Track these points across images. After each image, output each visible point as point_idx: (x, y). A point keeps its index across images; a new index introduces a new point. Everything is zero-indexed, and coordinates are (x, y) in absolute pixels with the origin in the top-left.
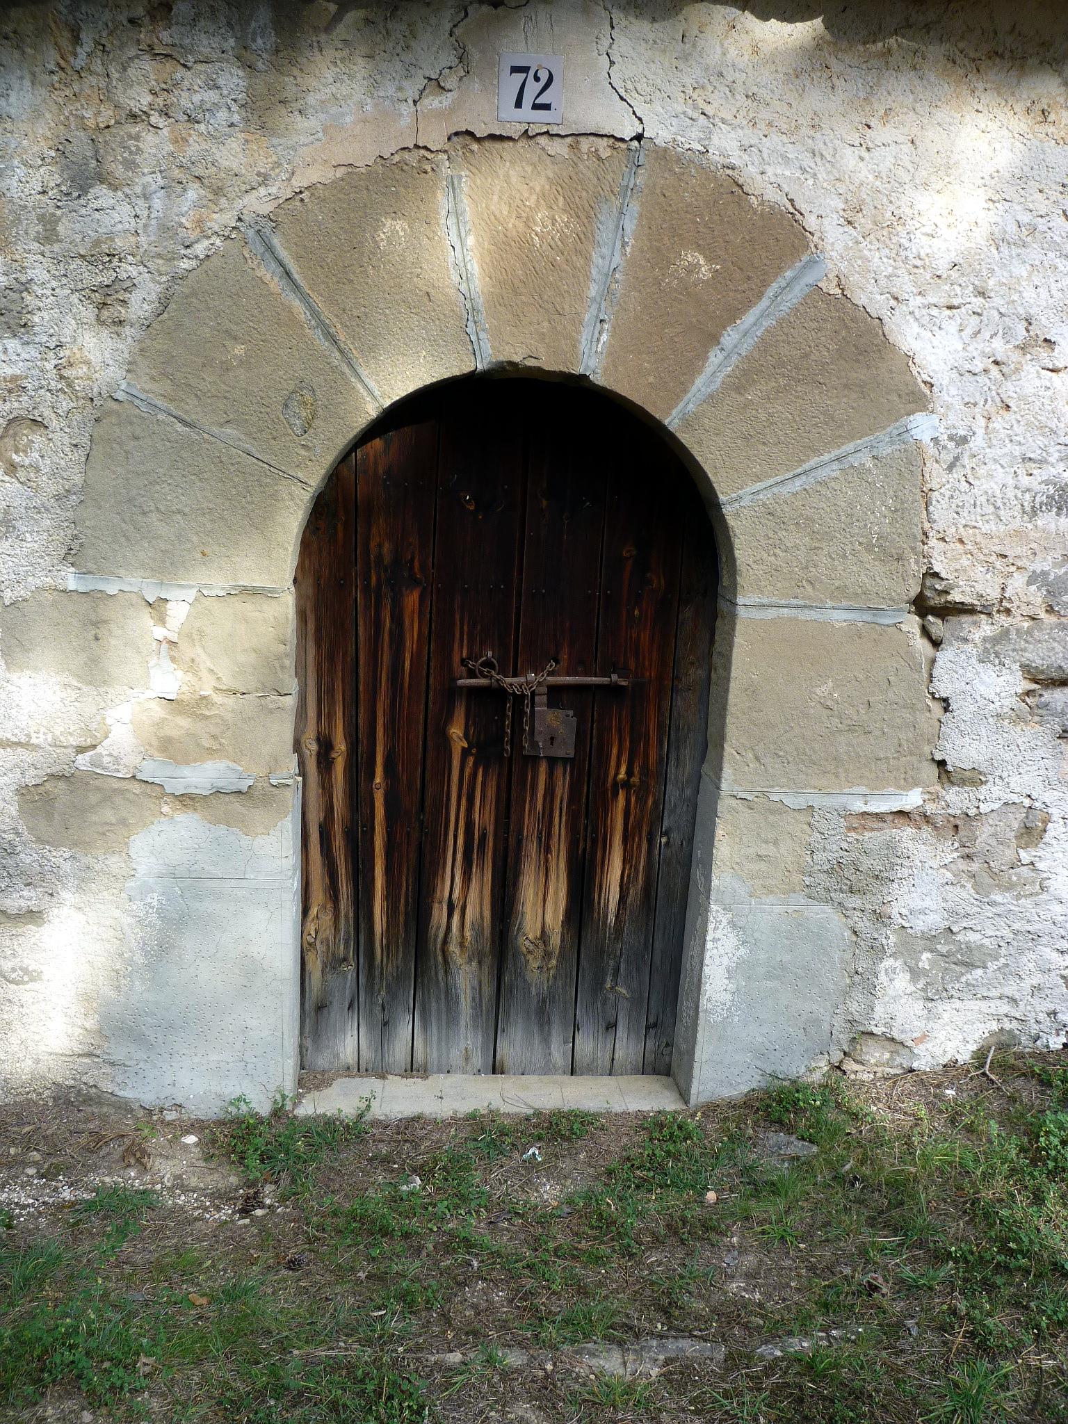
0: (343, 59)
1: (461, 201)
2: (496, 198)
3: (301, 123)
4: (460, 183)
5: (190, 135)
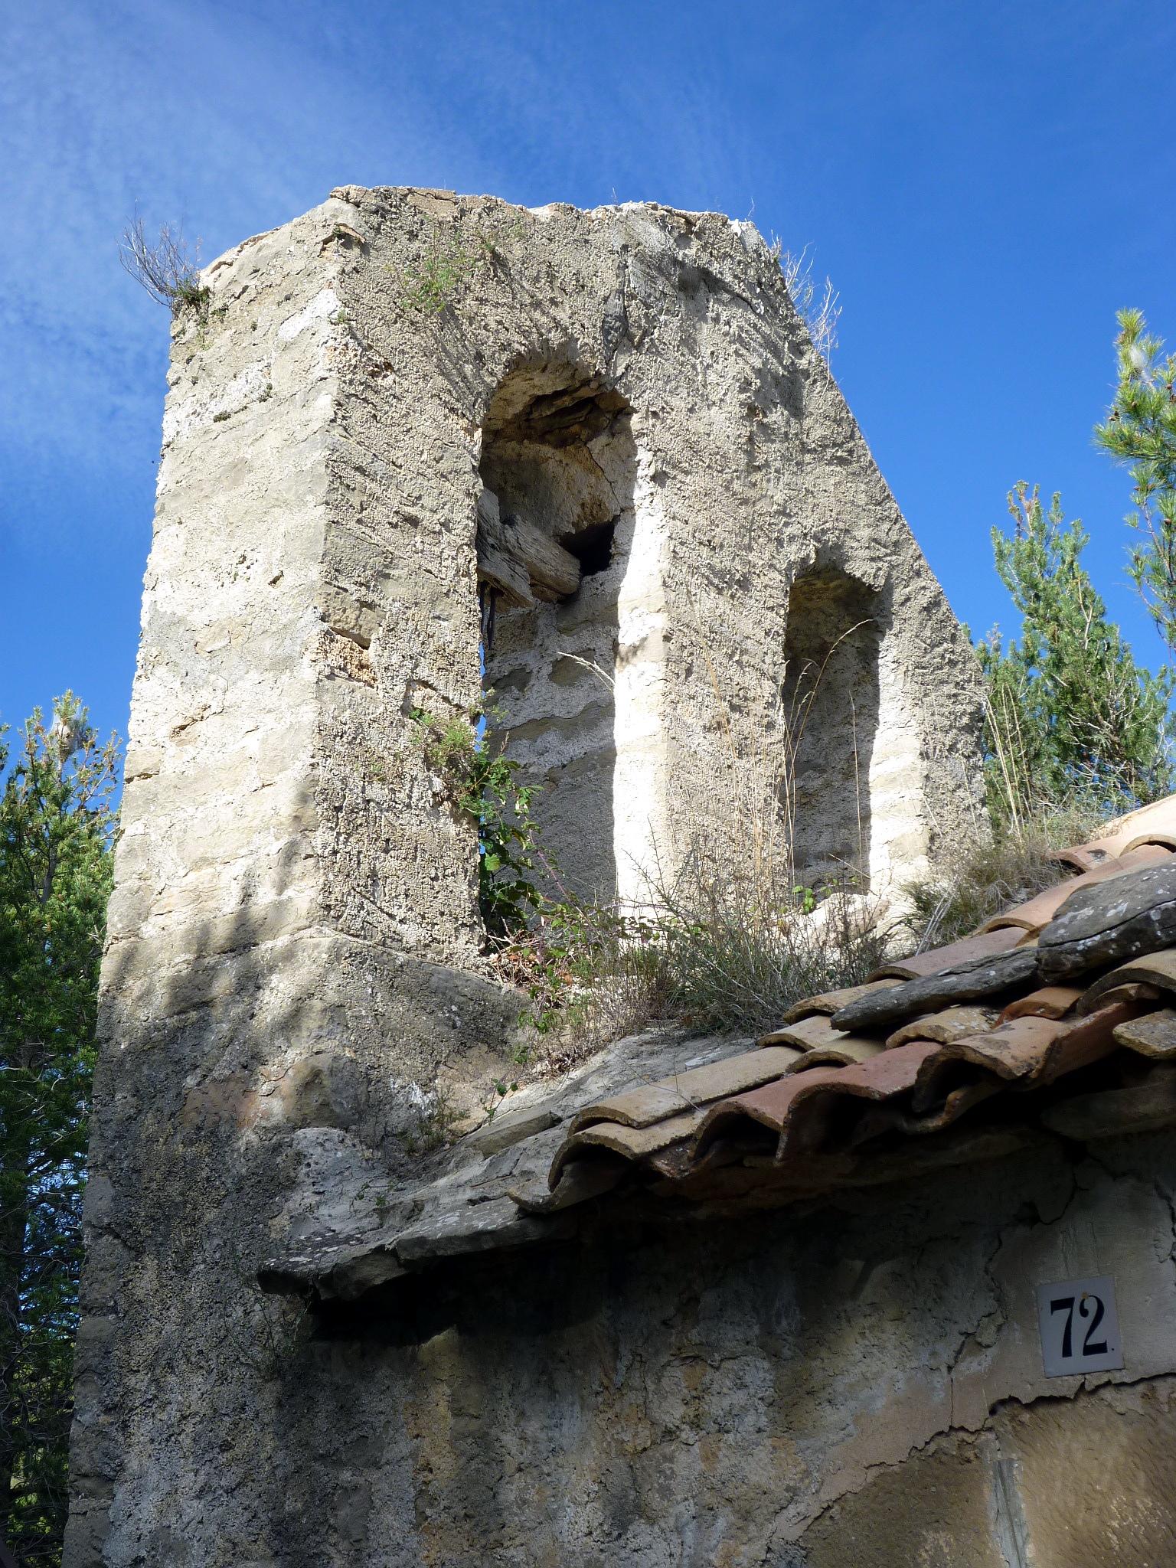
0: (872, 1328)
1: (1015, 1495)
2: (1058, 1484)
3: (831, 1416)
4: (1010, 1470)
5: (719, 1449)
